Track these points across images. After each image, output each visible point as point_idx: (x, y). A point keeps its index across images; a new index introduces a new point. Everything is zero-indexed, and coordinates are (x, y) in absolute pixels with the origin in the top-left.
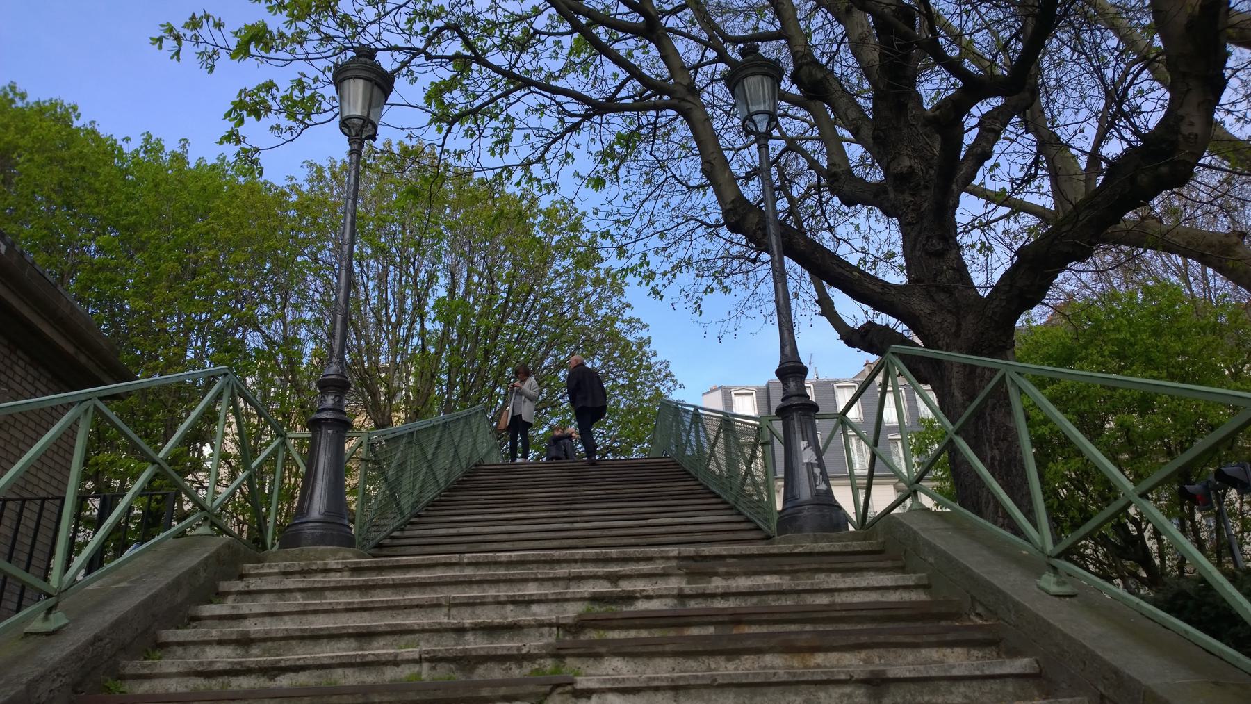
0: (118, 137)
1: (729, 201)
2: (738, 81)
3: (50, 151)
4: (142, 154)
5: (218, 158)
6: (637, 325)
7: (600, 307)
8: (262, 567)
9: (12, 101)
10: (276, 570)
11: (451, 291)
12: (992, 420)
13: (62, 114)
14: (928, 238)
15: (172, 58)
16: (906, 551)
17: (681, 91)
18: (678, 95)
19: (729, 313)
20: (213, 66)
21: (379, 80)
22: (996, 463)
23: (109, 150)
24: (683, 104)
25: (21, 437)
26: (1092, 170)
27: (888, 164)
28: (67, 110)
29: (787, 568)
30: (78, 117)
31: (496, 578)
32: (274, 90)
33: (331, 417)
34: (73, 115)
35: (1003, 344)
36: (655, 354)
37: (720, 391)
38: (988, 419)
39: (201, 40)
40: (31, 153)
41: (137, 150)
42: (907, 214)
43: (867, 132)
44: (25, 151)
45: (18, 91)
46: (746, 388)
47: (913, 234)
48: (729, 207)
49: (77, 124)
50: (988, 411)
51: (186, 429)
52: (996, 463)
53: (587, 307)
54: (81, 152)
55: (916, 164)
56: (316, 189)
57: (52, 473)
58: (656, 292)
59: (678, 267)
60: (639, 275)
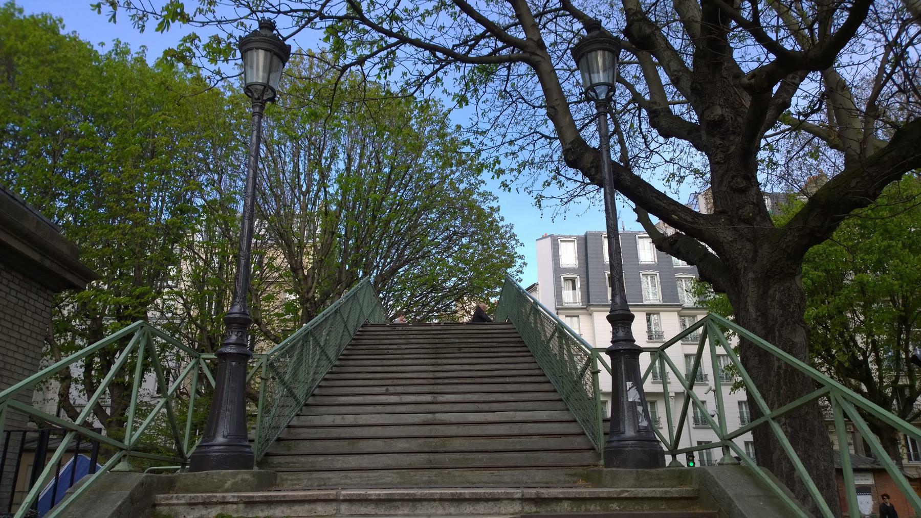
1: (569, 141)
2: (583, 55)
4: (113, 56)
6: (490, 197)
7: (461, 181)
9: (13, 15)
10: (183, 501)
11: (348, 169)
12: (780, 336)
13: (51, 25)
14: (733, 177)
15: (110, 21)
16: (720, 510)
17: (532, 46)
18: (530, 50)
20: (144, 26)
21: (277, 51)
22: (782, 372)
23: (91, 55)
24: (534, 57)
28: (54, 21)
30: (63, 27)
32: (197, 41)
34: (59, 26)
36: (502, 219)
37: (549, 239)
38: (777, 334)
39: (132, 6)
40: (28, 56)
41: (110, 52)
43: (686, 83)
44: (24, 54)
45: (16, 7)
46: (570, 237)
47: (721, 172)
48: (568, 146)
49: (63, 32)
50: (777, 327)
51: (112, 377)
52: (782, 372)
53: (451, 183)
54: (65, 56)
55: (727, 113)
57: (27, 353)
58: (504, 185)
59: (523, 165)
60: (492, 171)
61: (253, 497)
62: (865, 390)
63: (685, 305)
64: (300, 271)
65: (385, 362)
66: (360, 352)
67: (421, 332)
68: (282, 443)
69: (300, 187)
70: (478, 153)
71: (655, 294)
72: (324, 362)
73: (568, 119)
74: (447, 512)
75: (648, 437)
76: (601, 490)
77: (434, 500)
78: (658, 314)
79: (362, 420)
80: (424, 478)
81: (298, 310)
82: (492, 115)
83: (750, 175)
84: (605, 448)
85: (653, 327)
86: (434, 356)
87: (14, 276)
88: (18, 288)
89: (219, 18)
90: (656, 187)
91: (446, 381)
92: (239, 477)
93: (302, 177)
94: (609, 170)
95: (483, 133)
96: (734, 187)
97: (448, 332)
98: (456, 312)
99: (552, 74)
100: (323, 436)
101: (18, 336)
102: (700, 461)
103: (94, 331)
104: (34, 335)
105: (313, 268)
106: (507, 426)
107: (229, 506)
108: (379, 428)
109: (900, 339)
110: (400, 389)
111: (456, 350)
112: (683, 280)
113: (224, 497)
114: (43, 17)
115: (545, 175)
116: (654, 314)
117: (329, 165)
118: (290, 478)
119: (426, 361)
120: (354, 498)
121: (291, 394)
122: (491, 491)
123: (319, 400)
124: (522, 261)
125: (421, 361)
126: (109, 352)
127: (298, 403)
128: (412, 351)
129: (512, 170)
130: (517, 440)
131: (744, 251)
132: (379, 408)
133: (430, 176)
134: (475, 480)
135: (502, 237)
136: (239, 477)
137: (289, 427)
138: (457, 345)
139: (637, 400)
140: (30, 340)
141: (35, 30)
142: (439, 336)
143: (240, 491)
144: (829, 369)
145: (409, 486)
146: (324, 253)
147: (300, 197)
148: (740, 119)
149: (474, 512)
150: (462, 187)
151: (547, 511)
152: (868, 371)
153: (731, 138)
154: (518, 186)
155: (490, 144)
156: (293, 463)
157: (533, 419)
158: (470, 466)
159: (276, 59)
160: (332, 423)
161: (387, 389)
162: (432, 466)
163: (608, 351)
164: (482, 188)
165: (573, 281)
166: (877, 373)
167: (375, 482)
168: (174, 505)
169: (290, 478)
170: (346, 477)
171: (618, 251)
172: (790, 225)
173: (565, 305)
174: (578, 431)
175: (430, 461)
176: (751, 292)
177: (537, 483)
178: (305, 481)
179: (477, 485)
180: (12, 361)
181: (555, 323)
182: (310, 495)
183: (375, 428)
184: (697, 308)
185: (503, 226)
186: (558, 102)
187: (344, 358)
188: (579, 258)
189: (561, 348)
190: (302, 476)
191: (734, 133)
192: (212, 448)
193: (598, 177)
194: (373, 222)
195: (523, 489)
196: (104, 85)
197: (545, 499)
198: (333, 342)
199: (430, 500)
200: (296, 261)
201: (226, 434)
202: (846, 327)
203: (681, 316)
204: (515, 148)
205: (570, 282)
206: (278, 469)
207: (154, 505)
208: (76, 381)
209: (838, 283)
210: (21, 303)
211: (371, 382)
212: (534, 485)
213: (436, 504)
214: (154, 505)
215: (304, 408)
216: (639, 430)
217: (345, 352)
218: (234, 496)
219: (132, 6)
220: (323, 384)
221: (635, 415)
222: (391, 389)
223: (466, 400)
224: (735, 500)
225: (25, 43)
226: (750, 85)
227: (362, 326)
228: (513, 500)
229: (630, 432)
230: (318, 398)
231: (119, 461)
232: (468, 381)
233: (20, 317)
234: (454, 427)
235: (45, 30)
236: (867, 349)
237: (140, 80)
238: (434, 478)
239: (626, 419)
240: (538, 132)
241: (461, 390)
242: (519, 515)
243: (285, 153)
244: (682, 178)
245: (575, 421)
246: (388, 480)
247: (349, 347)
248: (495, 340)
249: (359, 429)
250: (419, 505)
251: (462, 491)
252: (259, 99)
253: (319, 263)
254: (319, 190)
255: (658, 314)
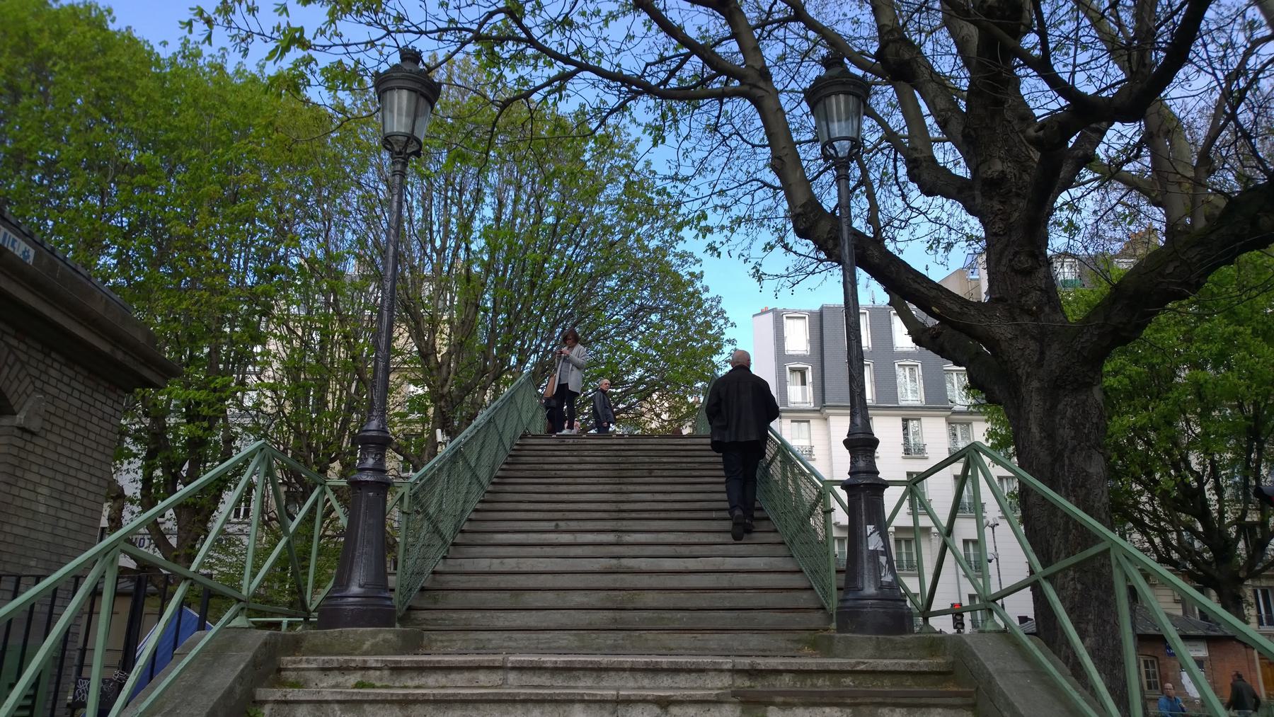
0: (155, 42)
3: (85, 59)
4: (179, 60)
5: (258, 65)
6: (690, 259)
8: (300, 661)
10: (314, 666)
11: (498, 219)
12: (1071, 465)
13: (96, 17)
14: (1016, 254)
16: (978, 688)
17: (753, 76)
19: (787, 269)
20: (247, 49)
21: (424, 91)
23: (150, 59)
25: (59, 441)
26: (1203, 170)
27: (978, 167)
28: (101, 13)
29: (848, 701)
30: (113, 21)
31: (540, 698)
32: (313, 65)
33: (372, 479)
35: (1090, 380)
36: (707, 289)
38: (1067, 462)
40: (67, 61)
41: (174, 54)
42: (994, 224)
43: (956, 127)
44: (60, 58)
46: (799, 312)
47: (999, 246)
48: (798, 210)
53: (638, 240)
54: (118, 61)
55: (1009, 168)
56: (359, 103)
57: (92, 471)
58: (712, 248)
59: (738, 221)
60: (696, 228)
61: (400, 662)
62: (1201, 529)
63: (957, 408)
64: (432, 358)
65: (553, 488)
66: (519, 474)
67: (599, 447)
68: (427, 594)
69: (432, 241)
70: (678, 204)
71: (915, 392)
72: (475, 488)
73: (798, 174)
74: (639, 684)
75: (892, 595)
76: (831, 661)
77: (624, 670)
78: (919, 419)
79: (527, 565)
80: (609, 642)
81: (427, 408)
82: (697, 156)
83: (1037, 252)
84: (838, 608)
85: (911, 437)
86: (617, 480)
87: (77, 373)
88: (82, 388)
89: (345, 41)
90: (913, 266)
91: (634, 515)
92: (380, 637)
93: (435, 228)
94: (850, 253)
95: (685, 179)
96: (1016, 267)
97: (634, 447)
98: (642, 414)
99: (779, 114)
100: (478, 585)
101: (81, 449)
102: (972, 621)
103: (154, 434)
104: (101, 448)
105: (449, 353)
106: (714, 576)
107: (371, 672)
108: (550, 577)
109: (1248, 459)
110: (574, 525)
111: (645, 473)
112: (955, 374)
113: (365, 661)
114: (86, 6)
115: (766, 236)
116: (913, 420)
117: (473, 213)
118: (440, 638)
119: (607, 488)
120: (525, 665)
121: (436, 530)
122: (694, 659)
123: (469, 538)
124: (734, 347)
125: (600, 488)
126: (175, 464)
127: (445, 542)
128: (589, 473)
129: (722, 228)
130: (726, 594)
131: (1028, 352)
132: (548, 550)
133: (608, 230)
134: (672, 646)
135: (706, 314)
136: (380, 637)
137: (434, 573)
138: (646, 467)
139: (880, 549)
140: (96, 455)
141: (75, 25)
142: (623, 453)
143: (381, 654)
144: (1151, 499)
145: (590, 652)
146: (465, 329)
147: (432, 252)
148: (1026, 177)
149: (673, 685)
150: (653, 244)
151: (763, 686)
152: (1205, 502)
153: (1014, 202)
154: (731, 248)
155: (693, 194)
156: (442, 619)
157: (746, 568)
158: (666, 627)
159: (422, 101)
160: (487, 569)
161: (557, 525)
162: (619, 627)
163: (845, 485)
164: (680, 247)
165: (803, 372)
166: (1217, 507)
167: (547, 645)
168: (303, 669)
169: (440, 638)
170: (510, 639)
171: (860, 357)
172: (1087, 319)
173: (791, 406)
174: (804, 584)
175: (616, 620)
176: (1035, 407)
177: (751, 650)
178: (459, 643)
179: (675, 652)
180: (75, 482)
181: (776, 443)
182: (471, 661)
183: (544, 576)
184: (971, 413)
185: (707, 299)
186: (786, 151)
187: (499, 482)
188: (811, 341)
189: (785, 476)
190: (455, 636)
191: (1018, 195)
192: (345, 600)
193: (836, 252)
194: (531, 292)
195: (733, 658)
196: (169, 101)
197: (761, 671)
198: (486, 460)
199: (619, 669)
200: (427, 343)
201: (362, 583)
202: (1176, 444)
203: (949, 424)
204: (727, 201)
205: (799, 375)
206: (425, 627)
207: (279, 670)
208: (132, 502)
209: (1166, 383)
210: (85, 407)
211: (536, 515)
212: (748, 653)
213: (627, 674)
214: (279, 670)
215: (451, 548)
216: (881, 586)
217: (499, 473)
218: (377, 661)
219: (233, 25)
220: (473, 516)
221: (877, 568)
222: (563, 525)
223: (660, 541)
224: (995, 676)
225: (62, 43)
226: (1037, 138)
227: (521, 438)
228: (722, 671)
229: (870, 589)
230: (468, 536)
231: (237, 615)
232: (663, 515)
233: (84, 425)
234: (646, 577)
235: (88, 24)
236: (1203, 473)
237: (219, 96)
238: (621, 642)
239: (866, 572)
240: (758, 180)
241: (653, 528)
242: (729, 691)
243: (412, 196)
244: (949, 246)
245: (801, 571)
246: (564, 643)
247: (504, 467)
248: (698, 460)
249: (523, 577)
250: (604, 675)
251: (659, 659)
252: (400, 153)
253: (458, 348)
254: (458, 247)
255: (919, 419)
